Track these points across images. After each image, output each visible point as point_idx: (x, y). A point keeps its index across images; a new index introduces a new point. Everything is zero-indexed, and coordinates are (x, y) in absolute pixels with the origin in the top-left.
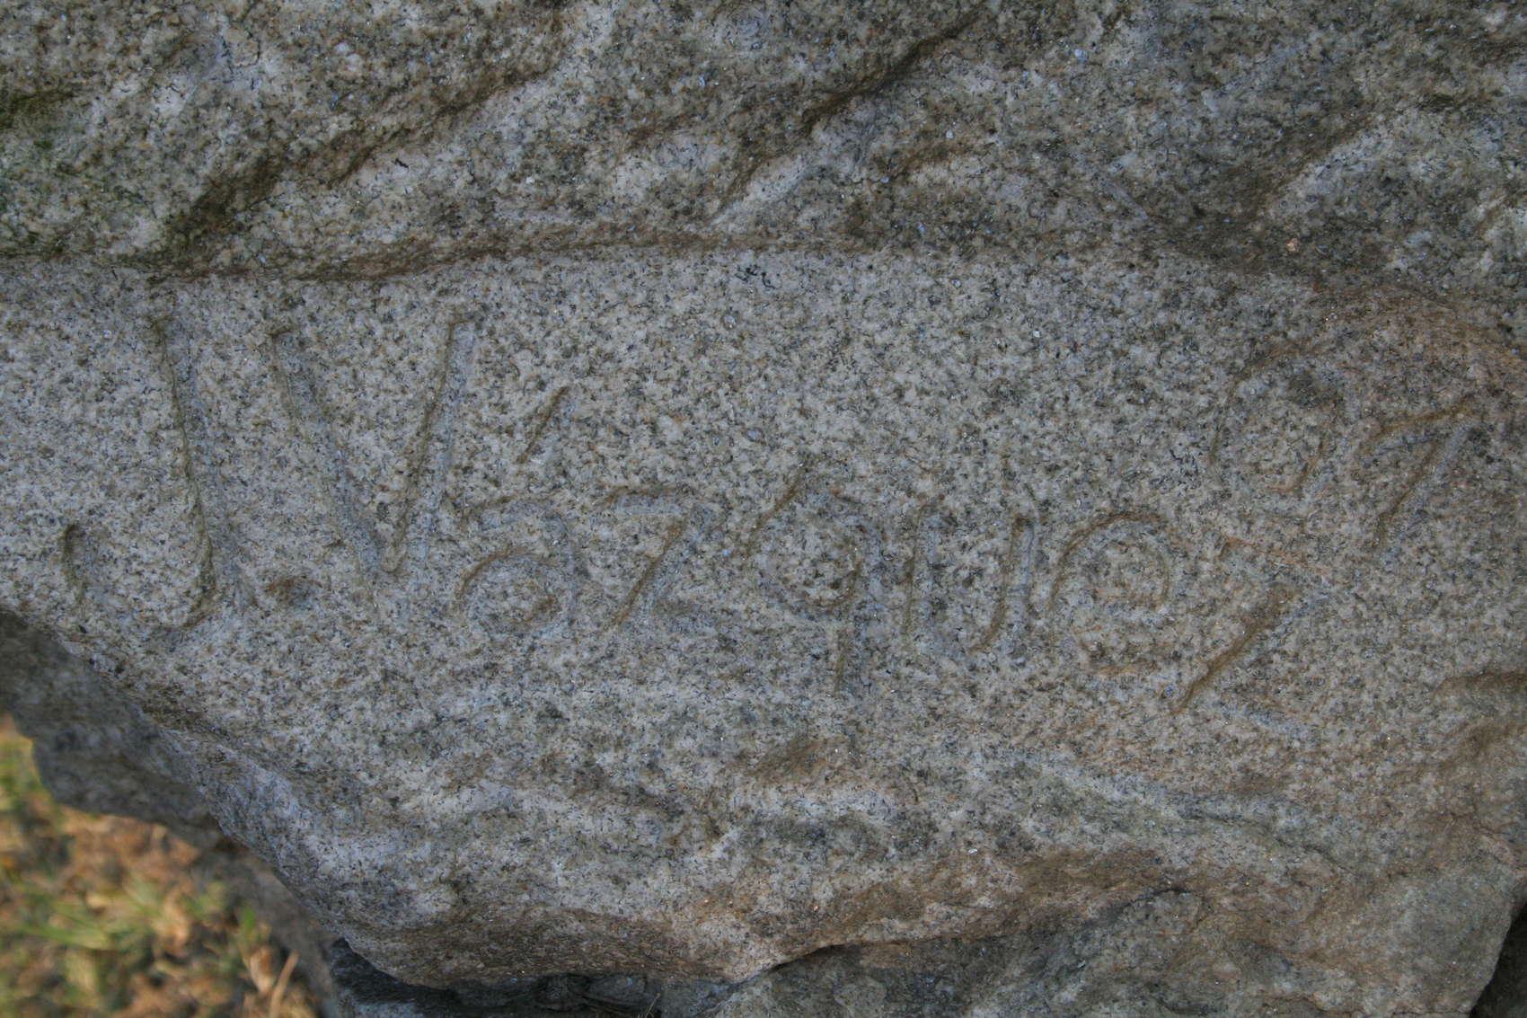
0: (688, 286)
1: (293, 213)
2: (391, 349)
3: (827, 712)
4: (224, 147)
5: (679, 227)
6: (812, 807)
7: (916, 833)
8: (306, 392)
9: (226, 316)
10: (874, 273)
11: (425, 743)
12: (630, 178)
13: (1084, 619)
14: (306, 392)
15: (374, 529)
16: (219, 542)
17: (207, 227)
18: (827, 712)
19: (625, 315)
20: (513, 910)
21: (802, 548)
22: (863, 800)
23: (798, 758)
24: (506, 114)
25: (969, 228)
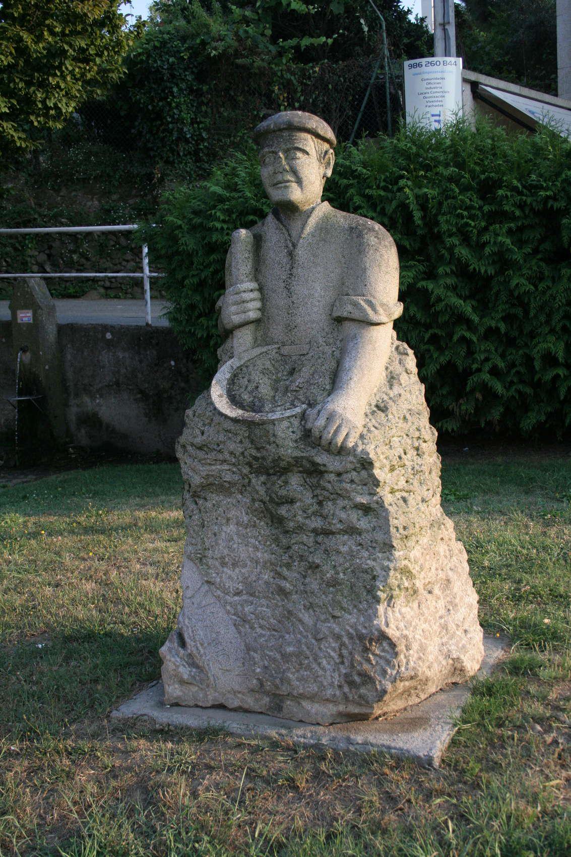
0: (225, 616)
1: (213, 587)
2: (210, 599)
3: (206, 645)
4: (212, 580)
5: (228, 613)
6: (200, 648)
7: (201, 656)
8: (205, 596)
9: (206, 587)
10: (233, 628)
11: (189, 619)
12: (228, 608)
13: (220, 658)
14: (205, 596)
15: (199, 606)
16: (193, 597)
17: (208, 582)
18: (206, 645)
19: (221, 614)
20: (472, 113)
21: (214, 635)
22: (202, 652)
23: (202, 645)
24: (227, 597)
25: (240, 633)
